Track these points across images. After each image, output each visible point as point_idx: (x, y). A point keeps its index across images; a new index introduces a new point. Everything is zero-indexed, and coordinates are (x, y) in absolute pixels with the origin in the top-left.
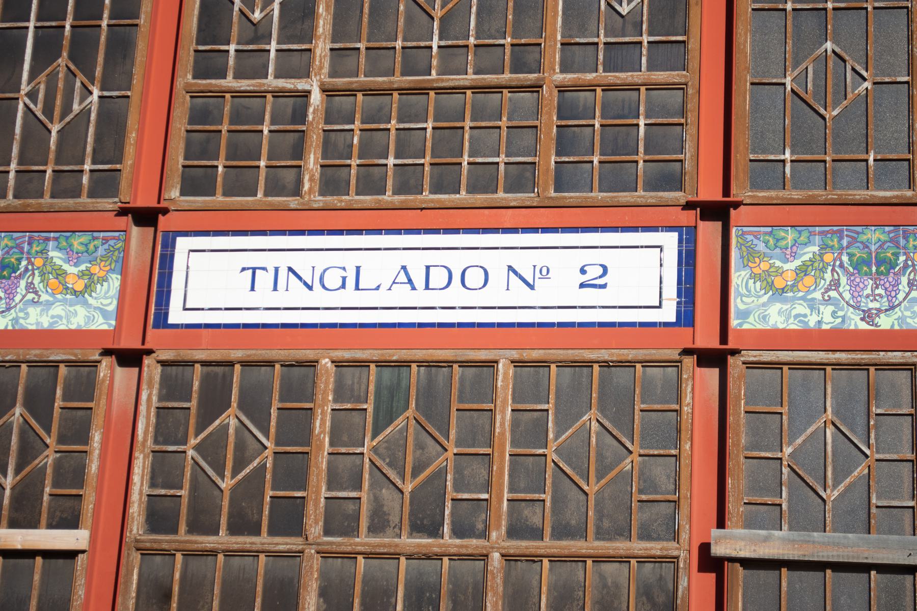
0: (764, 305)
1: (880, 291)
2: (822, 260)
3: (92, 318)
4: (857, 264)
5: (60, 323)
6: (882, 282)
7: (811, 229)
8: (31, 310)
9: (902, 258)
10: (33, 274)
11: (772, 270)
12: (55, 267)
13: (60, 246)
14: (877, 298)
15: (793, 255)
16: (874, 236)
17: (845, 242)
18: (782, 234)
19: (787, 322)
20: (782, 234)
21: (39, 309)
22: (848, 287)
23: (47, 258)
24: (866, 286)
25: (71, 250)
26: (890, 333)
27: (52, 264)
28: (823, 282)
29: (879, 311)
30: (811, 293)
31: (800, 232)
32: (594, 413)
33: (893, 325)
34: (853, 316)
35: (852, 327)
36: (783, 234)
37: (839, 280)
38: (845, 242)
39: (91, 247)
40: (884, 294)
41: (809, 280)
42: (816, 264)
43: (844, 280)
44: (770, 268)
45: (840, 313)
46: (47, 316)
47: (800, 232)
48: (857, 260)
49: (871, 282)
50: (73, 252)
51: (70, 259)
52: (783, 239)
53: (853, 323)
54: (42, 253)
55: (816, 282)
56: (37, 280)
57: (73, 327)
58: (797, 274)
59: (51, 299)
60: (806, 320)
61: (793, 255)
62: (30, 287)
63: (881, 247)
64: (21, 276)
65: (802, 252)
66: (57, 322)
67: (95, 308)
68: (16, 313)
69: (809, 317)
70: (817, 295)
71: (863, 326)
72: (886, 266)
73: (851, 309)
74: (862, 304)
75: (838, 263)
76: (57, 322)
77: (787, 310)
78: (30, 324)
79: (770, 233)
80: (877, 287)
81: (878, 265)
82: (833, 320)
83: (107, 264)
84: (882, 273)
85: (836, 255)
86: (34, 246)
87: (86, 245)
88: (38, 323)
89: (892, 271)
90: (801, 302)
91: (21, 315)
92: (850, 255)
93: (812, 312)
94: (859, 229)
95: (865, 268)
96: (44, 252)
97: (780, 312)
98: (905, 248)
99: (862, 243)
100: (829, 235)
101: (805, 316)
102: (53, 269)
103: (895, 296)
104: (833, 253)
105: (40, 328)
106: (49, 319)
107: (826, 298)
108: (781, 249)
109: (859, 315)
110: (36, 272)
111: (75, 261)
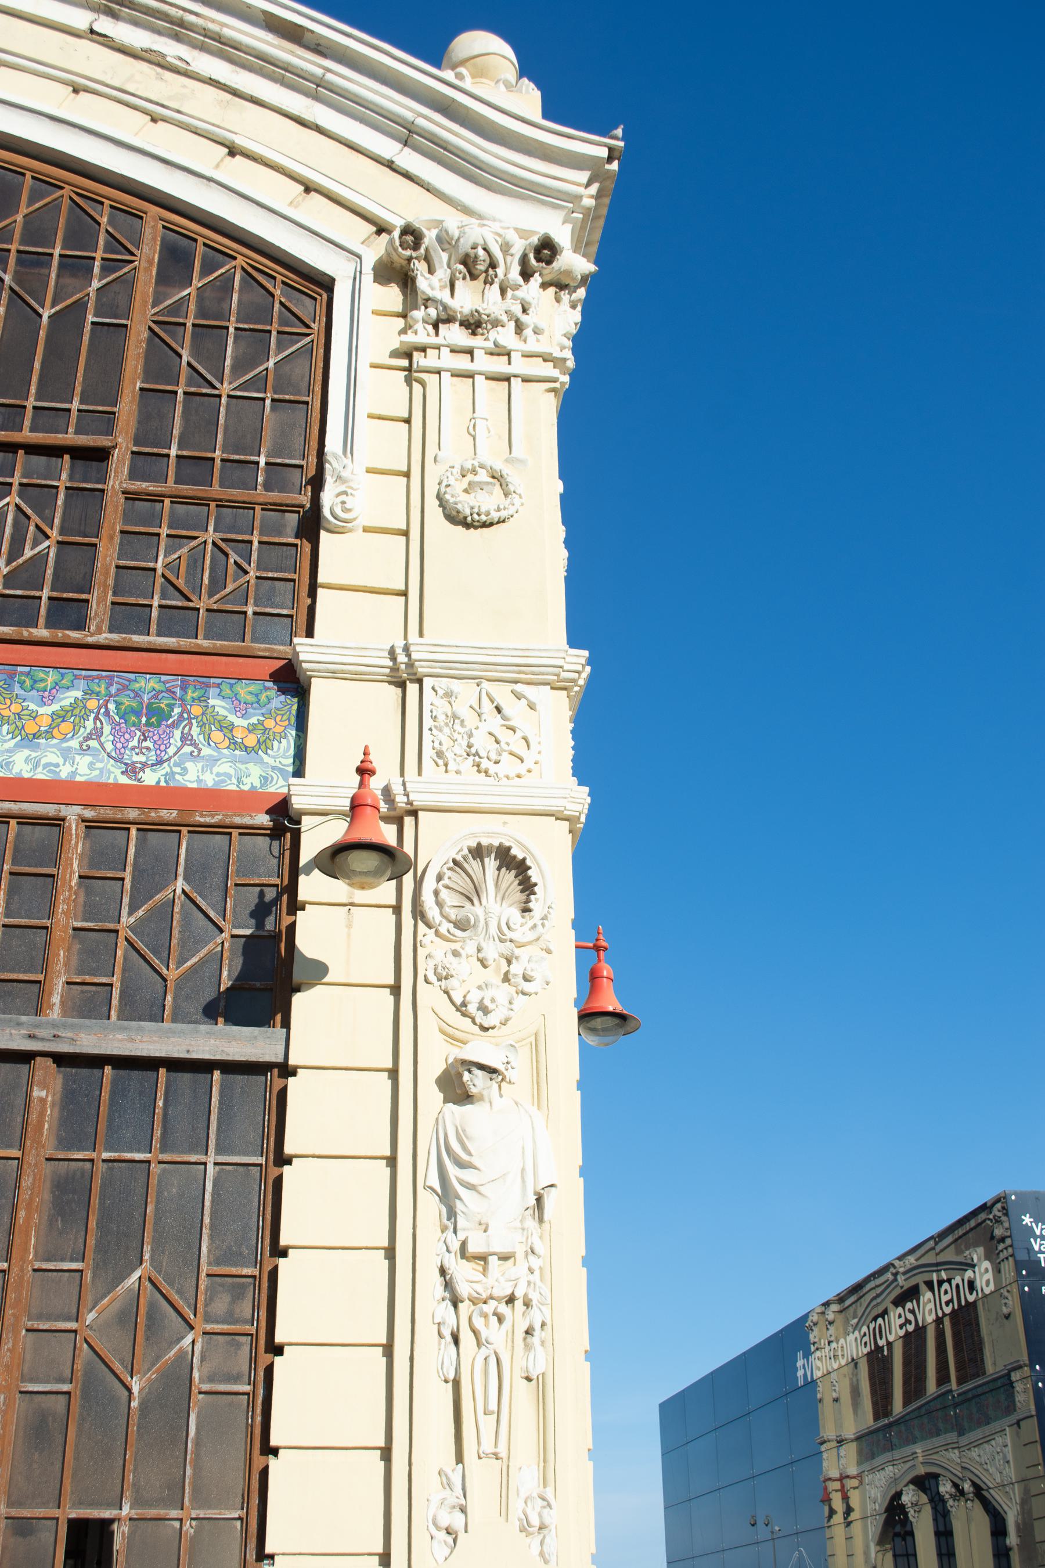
0: (9, 751)
1: (148, 744)
2: (85, 707)
3: (270, 779)
4: (125, 713)
5: (229, 782)
6: (151, 734)
7: (76, 672)
8: (189, 765)
9: (177, 710)
10: (190, 724)
11: (24, 712)
12: (219, 718)
13: (223, 694)
14: (144, 751)
15: (51, 698)
16: (148, 684)
17: (113, 689)
18: (42, 675)
19: (35, 771)
20: (42, 675)
21: (200, 765)
22: (111, 738)
23: (207, 706)
24: (132, 737)
25: (237, 699)
26: (156, 790)
27: (214, 714)
28: (82, 730)
29: (145, 765)
30: (67, 741)
31: (63, 675)
32: (180, 884)
33: (159, 782)
34: (112, 769)
35: (111, 781)
36: (43, 675)
37: (102, 728)
38: (113, 689)
39: (263, 698)
40: (152, 747)
41: (66, 727)
42: (76, 712)
43: (107, 729)
44: (23, 710)
45: (99, 765)
46: (212, 773)
47: (63, 675)
48: (125, 709)
49: (138, 733)
50: (240, 702)
51: (238, 709)
52: (42, 680)
53: (112, 776)
54: (200, 701)
55: (74, 729)
56: (195, 731)
57: (246, 788)
58: (53, 720)
59: (215, 754)
60: (58, 770)
61: (51, 698)
62: (184, 738)
63: (155, 697)
64: (175, 725)
65: (62, 696)
66: (224, 781)
67: (273, 768)
68: (171, 768)
69: (61, 767)
70: (74, 744)
71: (124, 780)
72: (156, 716)
73: (112, 761)
74: (126, 757)
75: (103, 710)
76: (224, 781)
77: (35, 758)
78: (190, 781)
79: (28, 674)
80: (145, 740)
81: (149, 718)
82: (90, 772)
83: (285, 718)
84: (152, 725)
85: (101, 702)
86: (190, 692)
87: (257, 695)
88: (199, 781)
89: (164, 723)
90: (54, 750)
91: (177, 770)
92: (118, 704)
93: (65, 761)
94: (132, 676)
95: (133, 718)
96: (203, 700)
97: (27, 760)
98: (181, 699)
99: (133, 691)
100: (97, 681)
101: (57, 765)
102: (215, 719)
103: (165, 750)
104: (99, 700)
105: (203, 786)
106: (213, 776)
107: (84, 747)
108: (38, 691)
109: (121, 768)
110: (194, 721)
111: (244, 712)
